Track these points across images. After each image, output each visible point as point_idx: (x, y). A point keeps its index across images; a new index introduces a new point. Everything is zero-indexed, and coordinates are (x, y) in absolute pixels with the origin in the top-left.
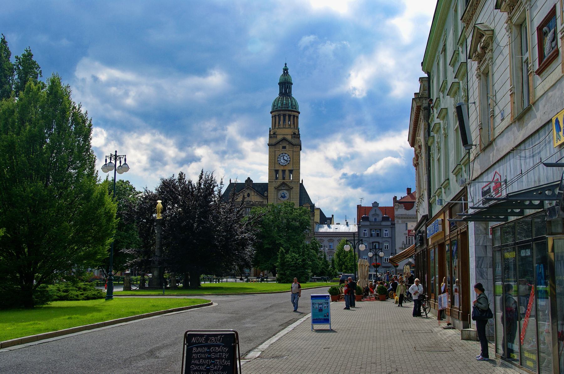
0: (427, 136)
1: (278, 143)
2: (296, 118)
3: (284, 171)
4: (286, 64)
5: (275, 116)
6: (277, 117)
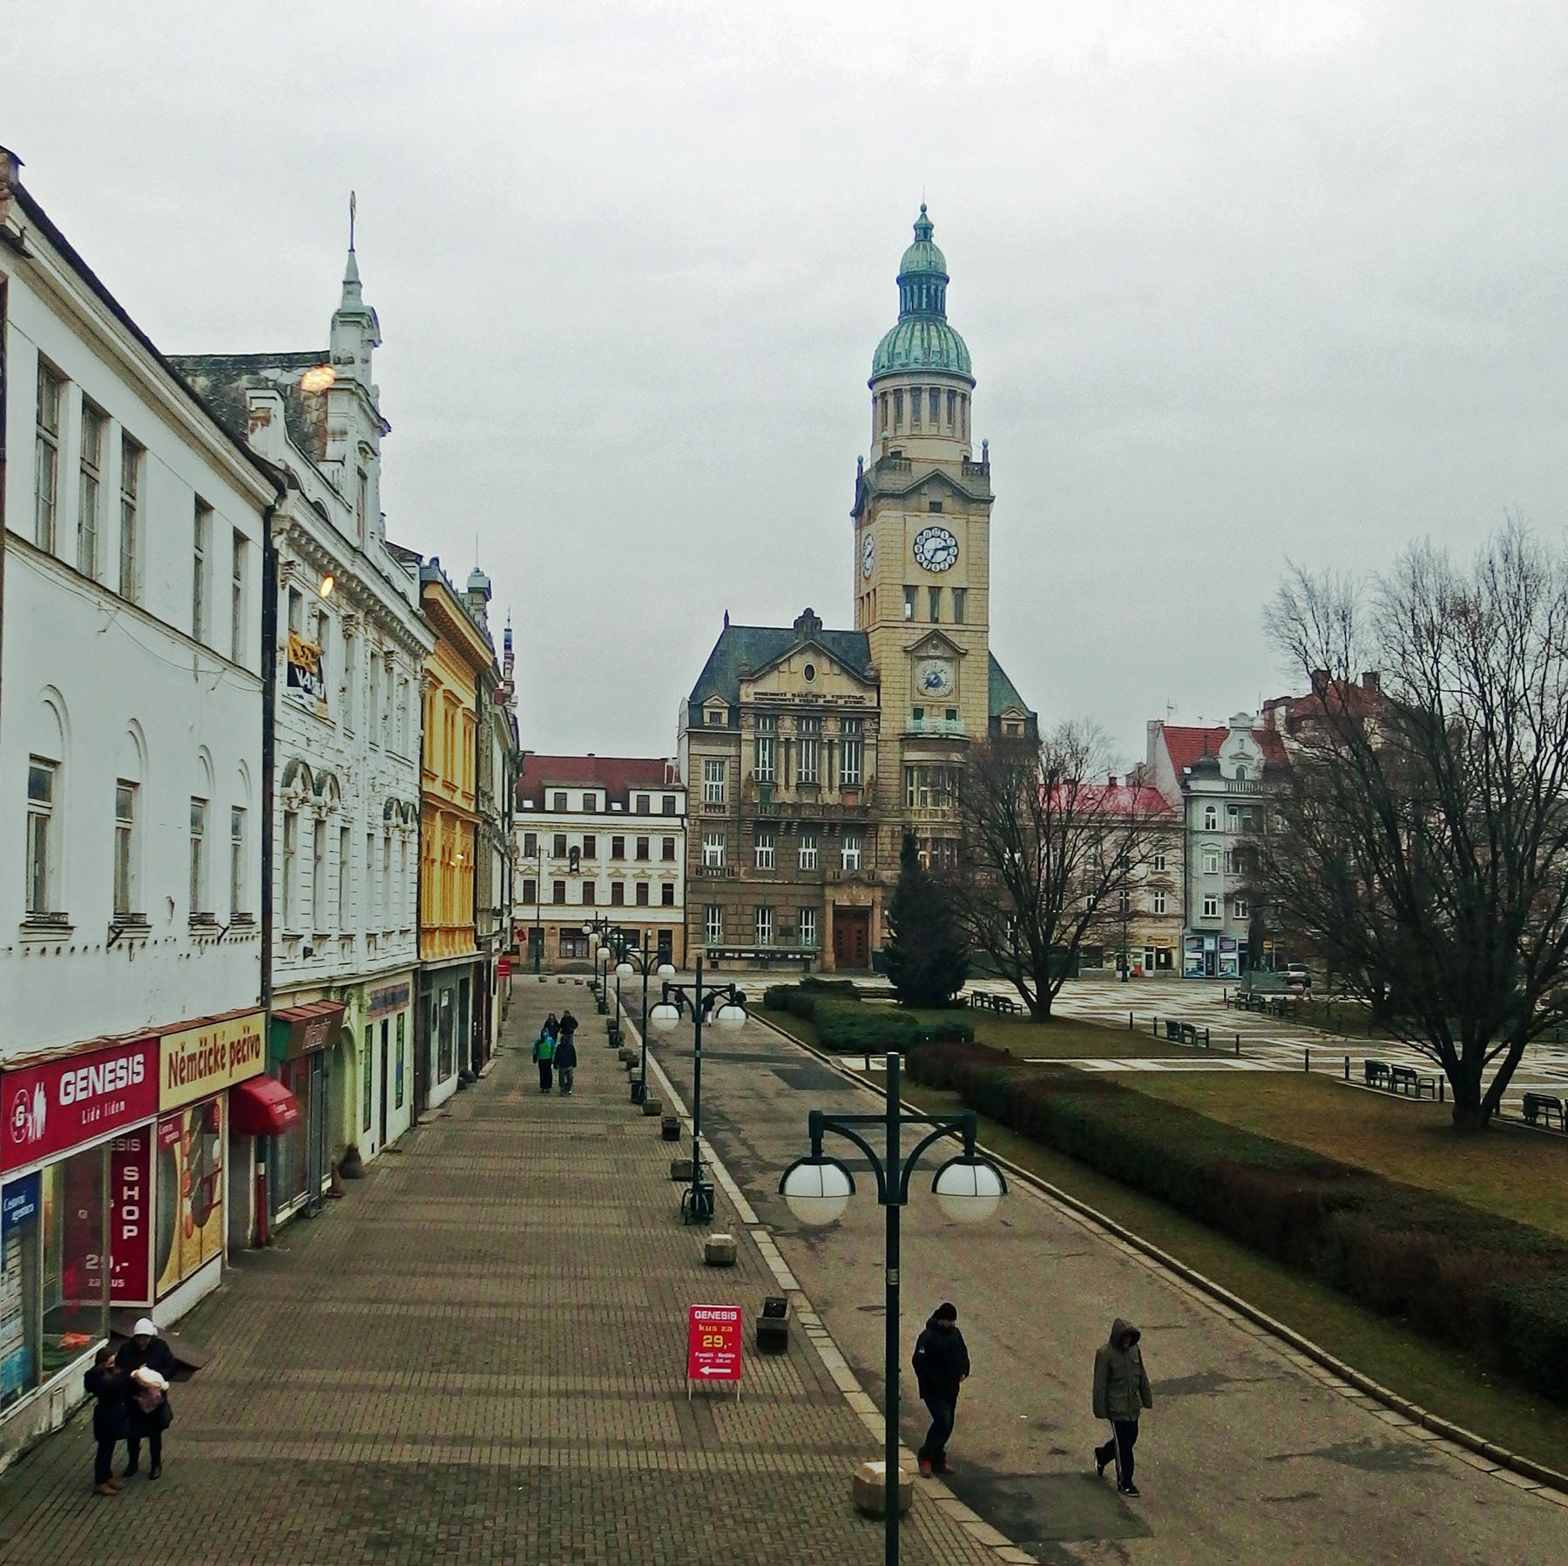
0: (879, 424)
1: (916, 490)
2: (958, 399)
3: (935, 591)
4: (924, 209)
5: (884, 394)
6: (891, 399)
